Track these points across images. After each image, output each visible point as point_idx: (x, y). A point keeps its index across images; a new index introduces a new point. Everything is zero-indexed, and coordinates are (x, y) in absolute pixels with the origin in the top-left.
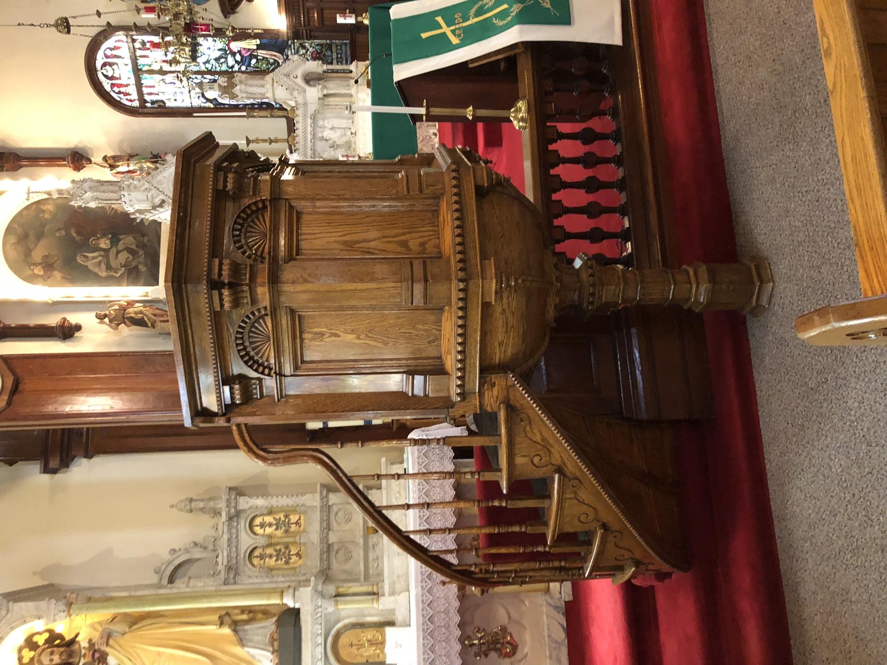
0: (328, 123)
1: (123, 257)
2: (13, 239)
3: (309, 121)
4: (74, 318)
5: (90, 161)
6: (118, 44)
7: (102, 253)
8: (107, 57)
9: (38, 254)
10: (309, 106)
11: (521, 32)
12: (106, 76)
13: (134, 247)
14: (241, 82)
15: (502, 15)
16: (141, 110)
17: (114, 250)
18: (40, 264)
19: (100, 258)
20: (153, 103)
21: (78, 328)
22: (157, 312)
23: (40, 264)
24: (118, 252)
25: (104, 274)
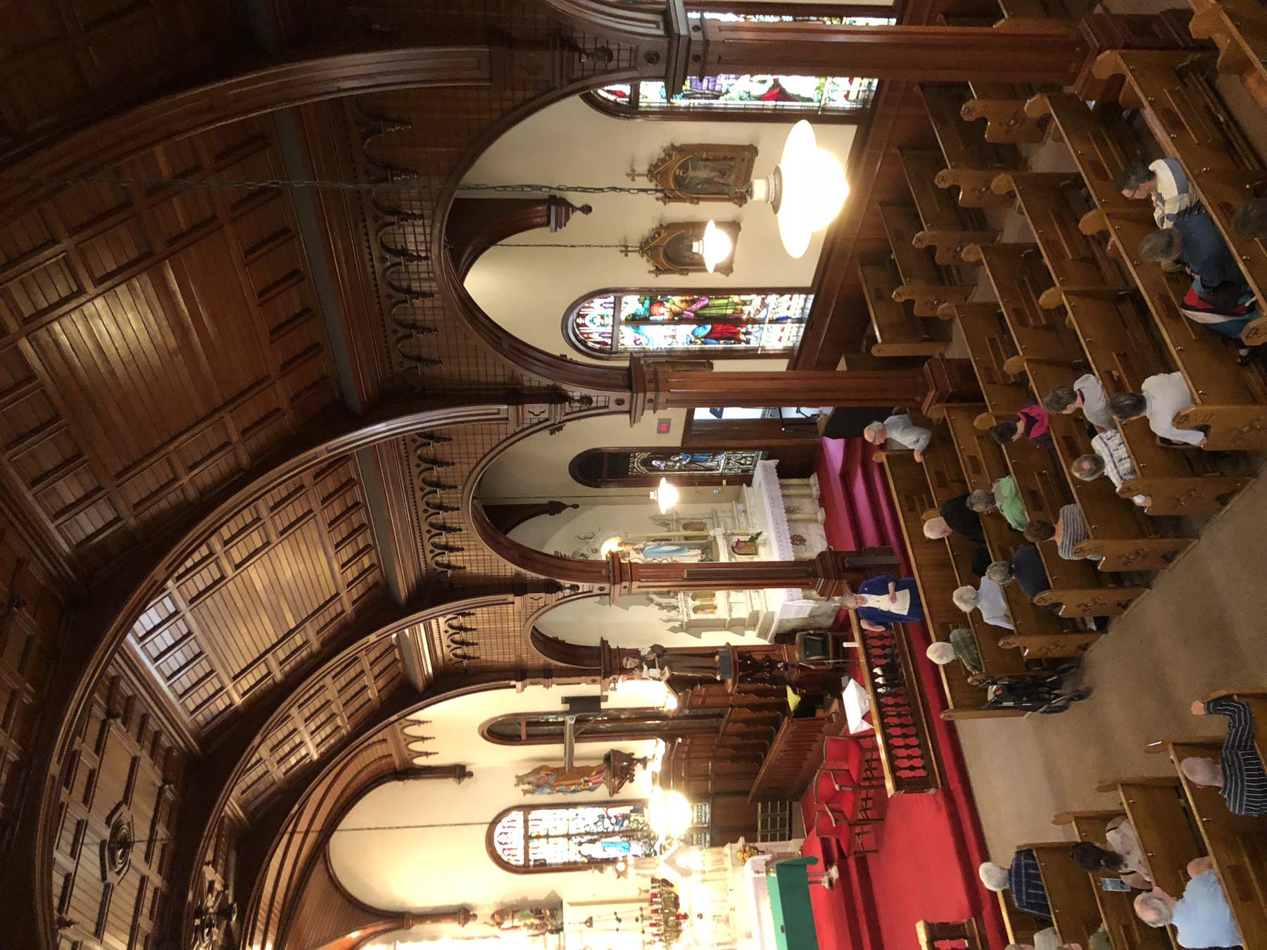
16: (525, 869)
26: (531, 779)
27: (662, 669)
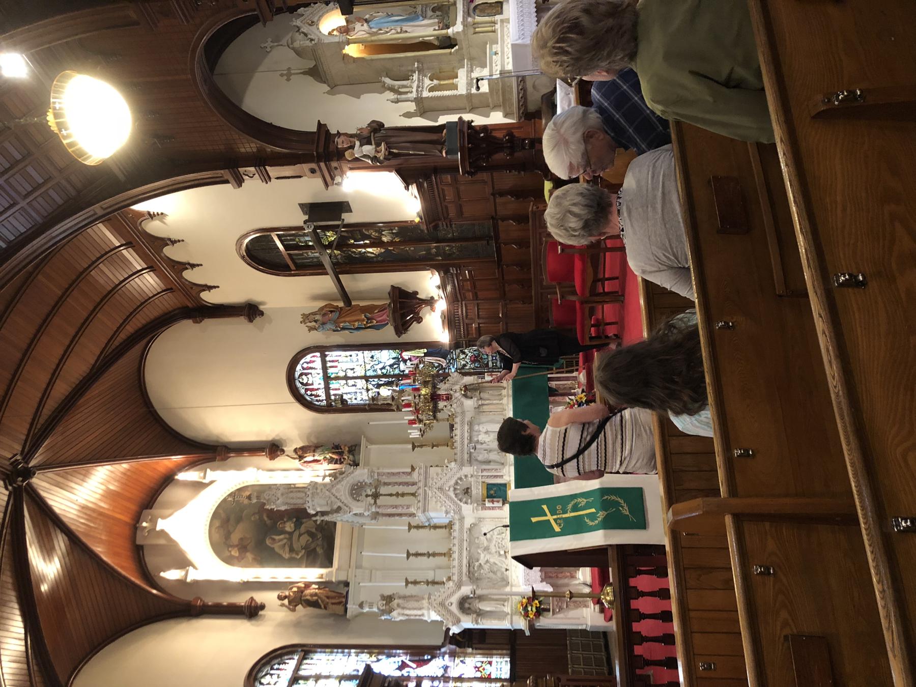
0: (483, 428)
1: (305, 539)
2: (217, 523)
3: (466, 427)
4: (260, 597)
5: (283, 451)
6: (313, 359)
7: (287, 536)
8: (304, 369)
9: (235, 537)
10: (467, 413)
11: (605, 536)
12: (302, 383)
13: (314, 530)
14: (398, 605)
15: (592, 516)
16: (328, 409)
17: (296, 534)
18: (237, 546)
19: (285, 541)
20: (335, 395)
21: (262, 607)
22: (330, 594)
23: (237, 546)
24: (300, 535)
25: (287, 556)
26: (318, 317)
27: (378, 145)
